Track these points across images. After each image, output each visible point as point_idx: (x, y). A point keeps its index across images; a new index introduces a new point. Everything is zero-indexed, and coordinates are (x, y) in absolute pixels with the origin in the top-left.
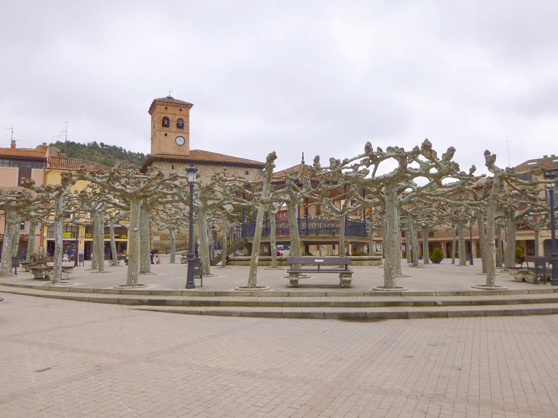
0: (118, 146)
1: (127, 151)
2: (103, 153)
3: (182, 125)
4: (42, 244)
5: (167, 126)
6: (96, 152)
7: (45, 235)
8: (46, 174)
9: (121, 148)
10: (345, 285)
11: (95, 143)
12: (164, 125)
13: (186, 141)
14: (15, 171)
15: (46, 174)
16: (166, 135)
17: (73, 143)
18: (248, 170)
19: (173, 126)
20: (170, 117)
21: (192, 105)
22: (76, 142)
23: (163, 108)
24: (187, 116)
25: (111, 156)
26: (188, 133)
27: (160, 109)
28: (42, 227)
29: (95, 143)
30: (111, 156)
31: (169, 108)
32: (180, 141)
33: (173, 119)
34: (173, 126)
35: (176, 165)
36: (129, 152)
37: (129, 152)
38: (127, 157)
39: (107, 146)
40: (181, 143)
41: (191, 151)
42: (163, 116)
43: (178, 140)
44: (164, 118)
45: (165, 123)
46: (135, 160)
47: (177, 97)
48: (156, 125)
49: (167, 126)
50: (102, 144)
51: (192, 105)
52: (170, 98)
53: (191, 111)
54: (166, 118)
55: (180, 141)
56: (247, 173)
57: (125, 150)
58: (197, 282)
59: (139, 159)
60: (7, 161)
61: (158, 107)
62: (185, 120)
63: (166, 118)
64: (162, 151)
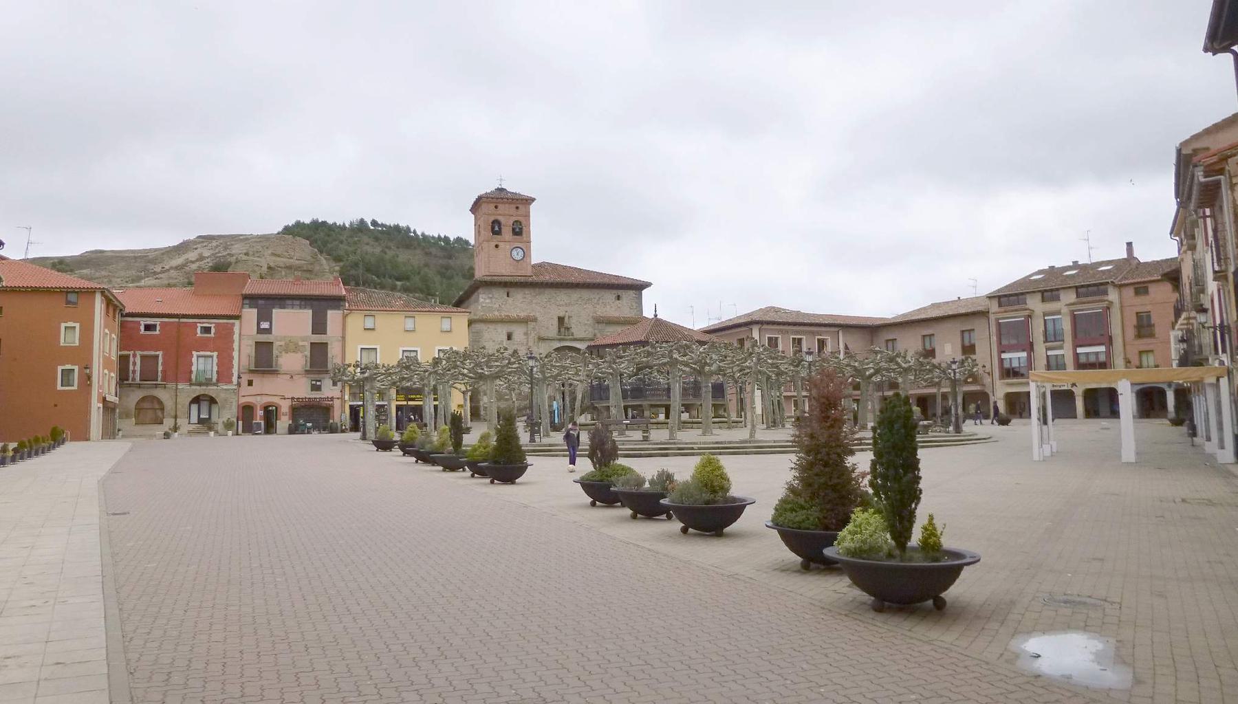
0: (403, 224)
1: (419, 233)
2: (377, 239)
3: (519, 230)
4: (343, 411)
5: (498, 233)
6: (365, 239)
7: (347, 397)
8: (345, 317)
9: (408, 228)
10: (646, 439)
11: (362, 221)
12: (495, 233)
13: (526, 254)
14: (307, 315)
15: (345, 317)
16: (497, 246)
17: (324, 223)
18: (620, 292)
19: (507, 233)
20: (500, 218)
21: (533, 200)
22: (330, 222)
23: (492, 206)
24: (527, 216)
25: (391, 244)
26: (529, 242)
27: (485, 208)
28: (343, 387)
29: (362, 221)
30: (391, 244)
31: (500, 206)
32: (518, 255)
33: (508, 223)
34: (507, 233)
35: (512, 290)
36: (423, 234)
37: (423, 234)
38: (419, 245)
39: (383, 225)
40: (519, 258)
41: (533, 266)
42: (492, 218)
43: (514, 253)
44: (493, 222)
45: (496, 228)
46: (433, 250)
47: (512, 187)
48: (482, 232)
49: (498, 233)
50: (374, 223)
51: (533, 200)
52: (501, 190)
53: (533, 207)
54: (496, 222)
55: (518, 255)
56: (618, 298)
57: (415, 232)
58: (537, 439)
59: (442, 248)
60: (298, 302)
61: (484, 206)
62: (524, 223)
63: (496, 222)
64: (503, 314)
